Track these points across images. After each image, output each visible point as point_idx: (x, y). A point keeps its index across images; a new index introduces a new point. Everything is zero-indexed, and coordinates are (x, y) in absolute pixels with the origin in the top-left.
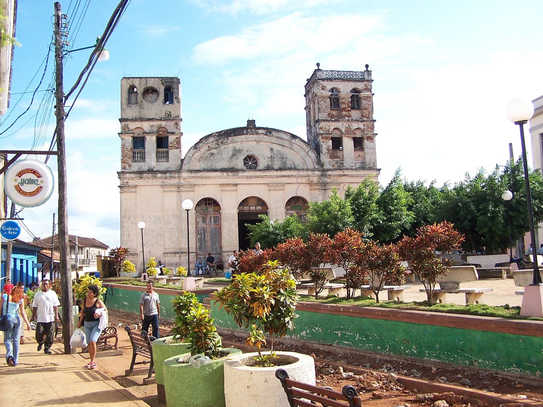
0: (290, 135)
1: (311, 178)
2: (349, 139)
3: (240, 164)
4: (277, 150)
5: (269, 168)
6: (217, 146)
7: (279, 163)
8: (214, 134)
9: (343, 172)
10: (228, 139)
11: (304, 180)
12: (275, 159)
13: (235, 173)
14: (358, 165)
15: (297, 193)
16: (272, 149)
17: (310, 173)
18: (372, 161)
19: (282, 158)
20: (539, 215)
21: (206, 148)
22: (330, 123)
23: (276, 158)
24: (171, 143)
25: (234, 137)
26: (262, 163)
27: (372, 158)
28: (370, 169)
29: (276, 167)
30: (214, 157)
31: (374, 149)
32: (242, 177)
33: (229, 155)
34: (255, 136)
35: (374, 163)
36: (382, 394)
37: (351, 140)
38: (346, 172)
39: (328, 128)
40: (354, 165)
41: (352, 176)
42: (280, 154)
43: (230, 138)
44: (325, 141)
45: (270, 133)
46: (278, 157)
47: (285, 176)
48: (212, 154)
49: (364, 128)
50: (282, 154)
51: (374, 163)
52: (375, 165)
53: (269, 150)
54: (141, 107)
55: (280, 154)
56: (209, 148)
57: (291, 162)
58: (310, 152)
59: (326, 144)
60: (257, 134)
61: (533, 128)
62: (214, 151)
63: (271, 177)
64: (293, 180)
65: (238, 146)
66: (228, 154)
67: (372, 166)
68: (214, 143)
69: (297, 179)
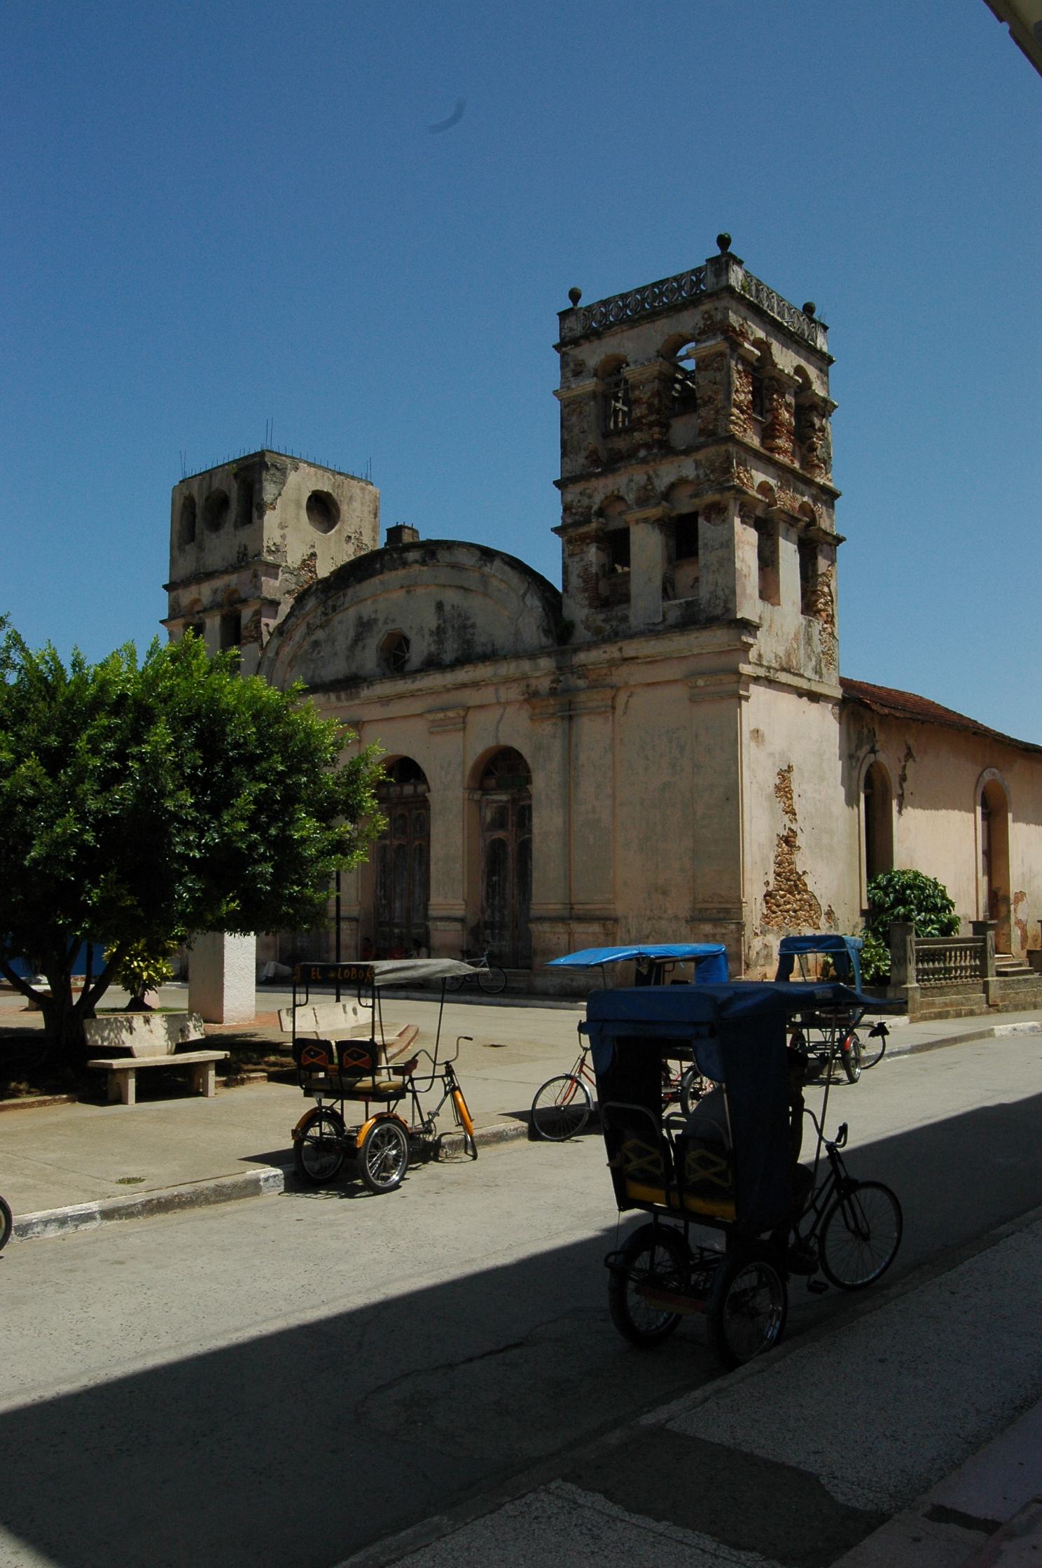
0: (478, 553)
1: (533, 682)
2: (650, 527)
3: (369, 658)
4: (453, 606)
5: (433, 664)
6: (324, 618)
7: (455, 646)
8: (314, 588)
9: (620, 649)
10: (344, 595)
11: (514, 693)
12: (448, 635)
13: (353, 690)
14: (673, 617)
15: (497, 737)
16: (440, 606)
17: (526, 666)
18: (720, 593)
19: (464, 626)
20: (345, 802)
21: (303, 629)
22: (594, 483)
23: (450, 632)
24: (246, 628)
25: (358, 587)
26: (419, 650)
27: (720, 581)
28: (711, 622)
29: (448, 657)
30: (319, 652)
31: (728, 547)
32: (369, 702)
33: (350, 639)
34: (401, 573)
35: (726, 602)
36: (118, 1277)
37: (654, 528)
38: (631, 648)
39: (586, 502)
40: (660, 619)
41: (652, 661)
42: (460, 615)
43: (350, 592)
44: (577, 550)
45: (433, 554)
46: (453, 627)
47: (464, 686)
48: (316, 644)
49: (698, 476)
50: (463, 615)
51: (726, 602)
52: (730, 606)
53: (433, 610)
54: (201, 548)
55: (460, 615)
56: (310, 629)
57: (483, 639)
58: (528, 596)
59: (582, 560)
60: (405, 564)
61: (568, 478)
62: (320, 635)
63: (432, 692)
64: (487, 695)
65: (367, 610)
66: (347, 639)
67: (719, 611)
68: (319, 612)
69: (497, 690)
